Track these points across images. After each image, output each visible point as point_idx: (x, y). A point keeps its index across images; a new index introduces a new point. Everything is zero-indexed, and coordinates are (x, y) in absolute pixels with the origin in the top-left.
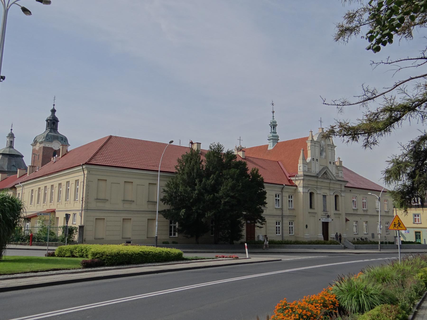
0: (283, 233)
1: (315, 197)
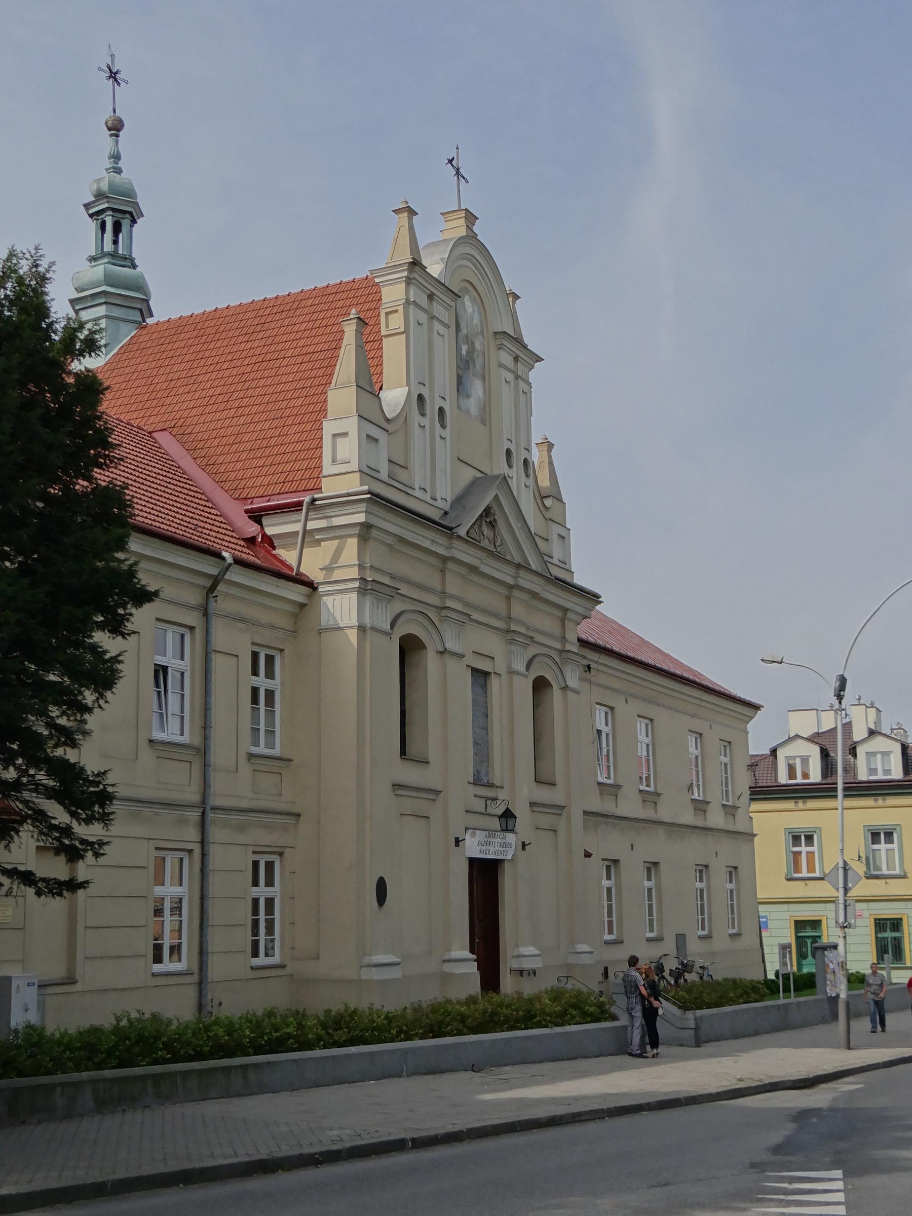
0: (202, 952)
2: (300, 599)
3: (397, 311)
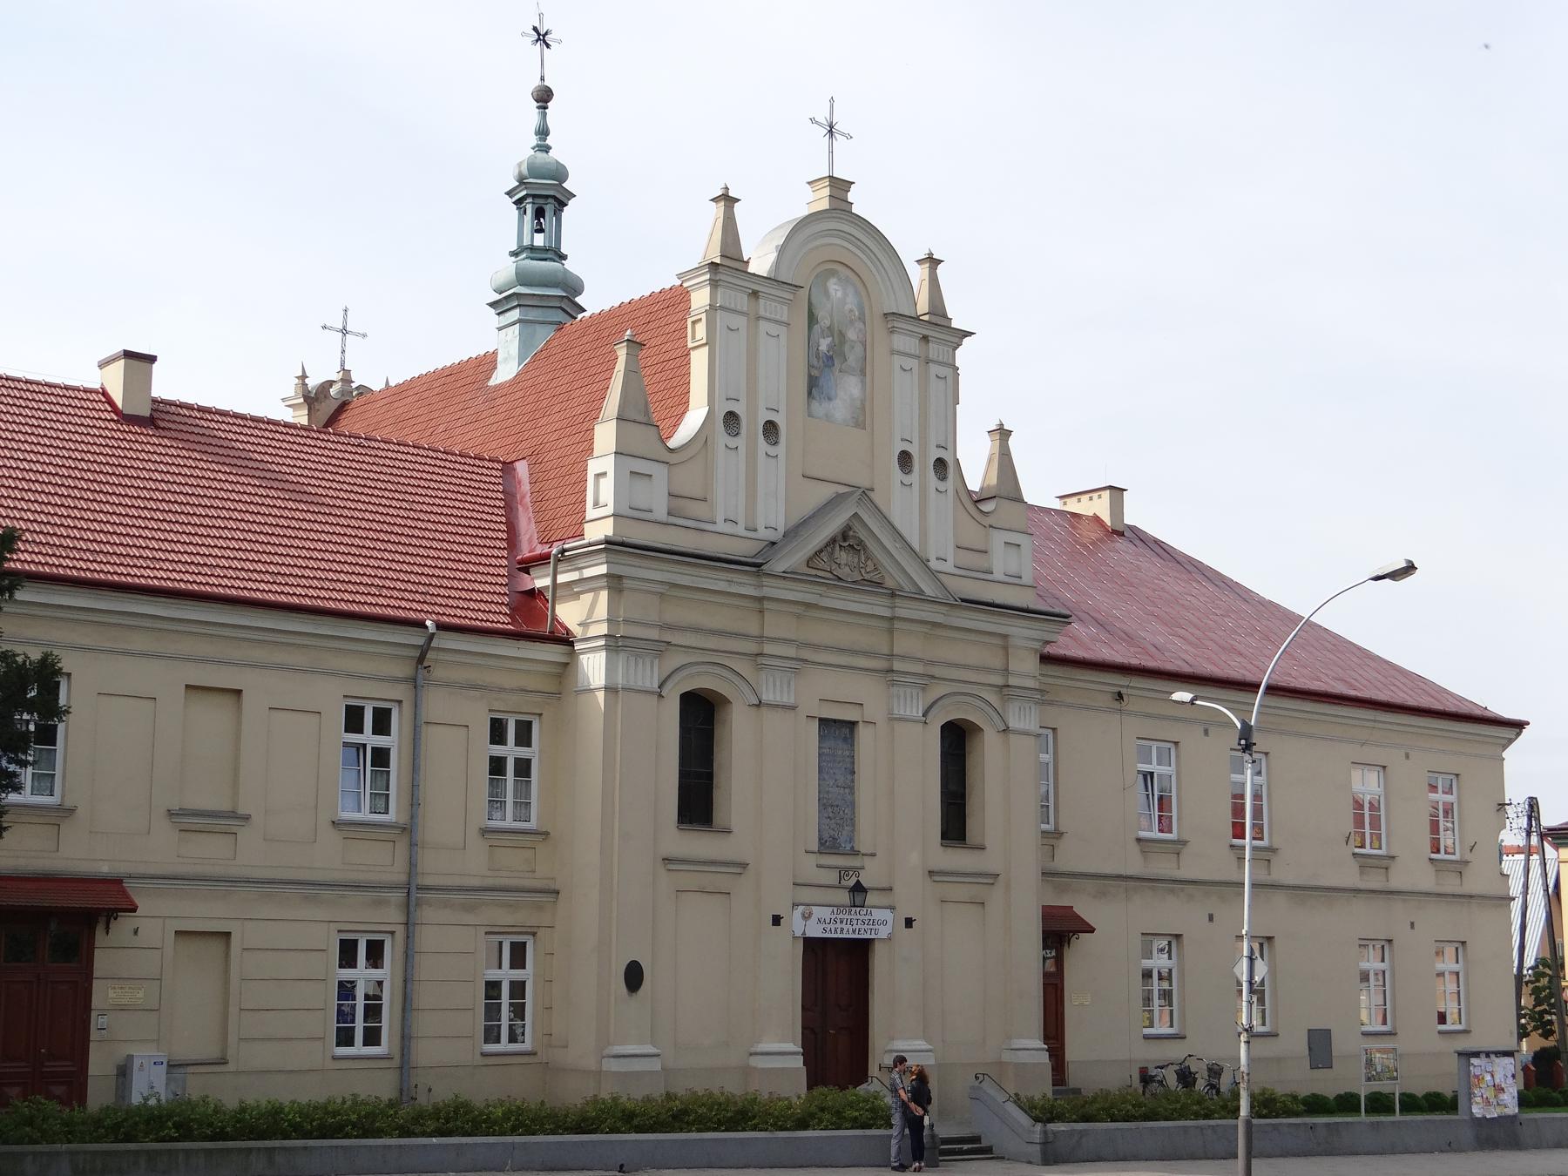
1: (740, 736)
2: (563, 659)
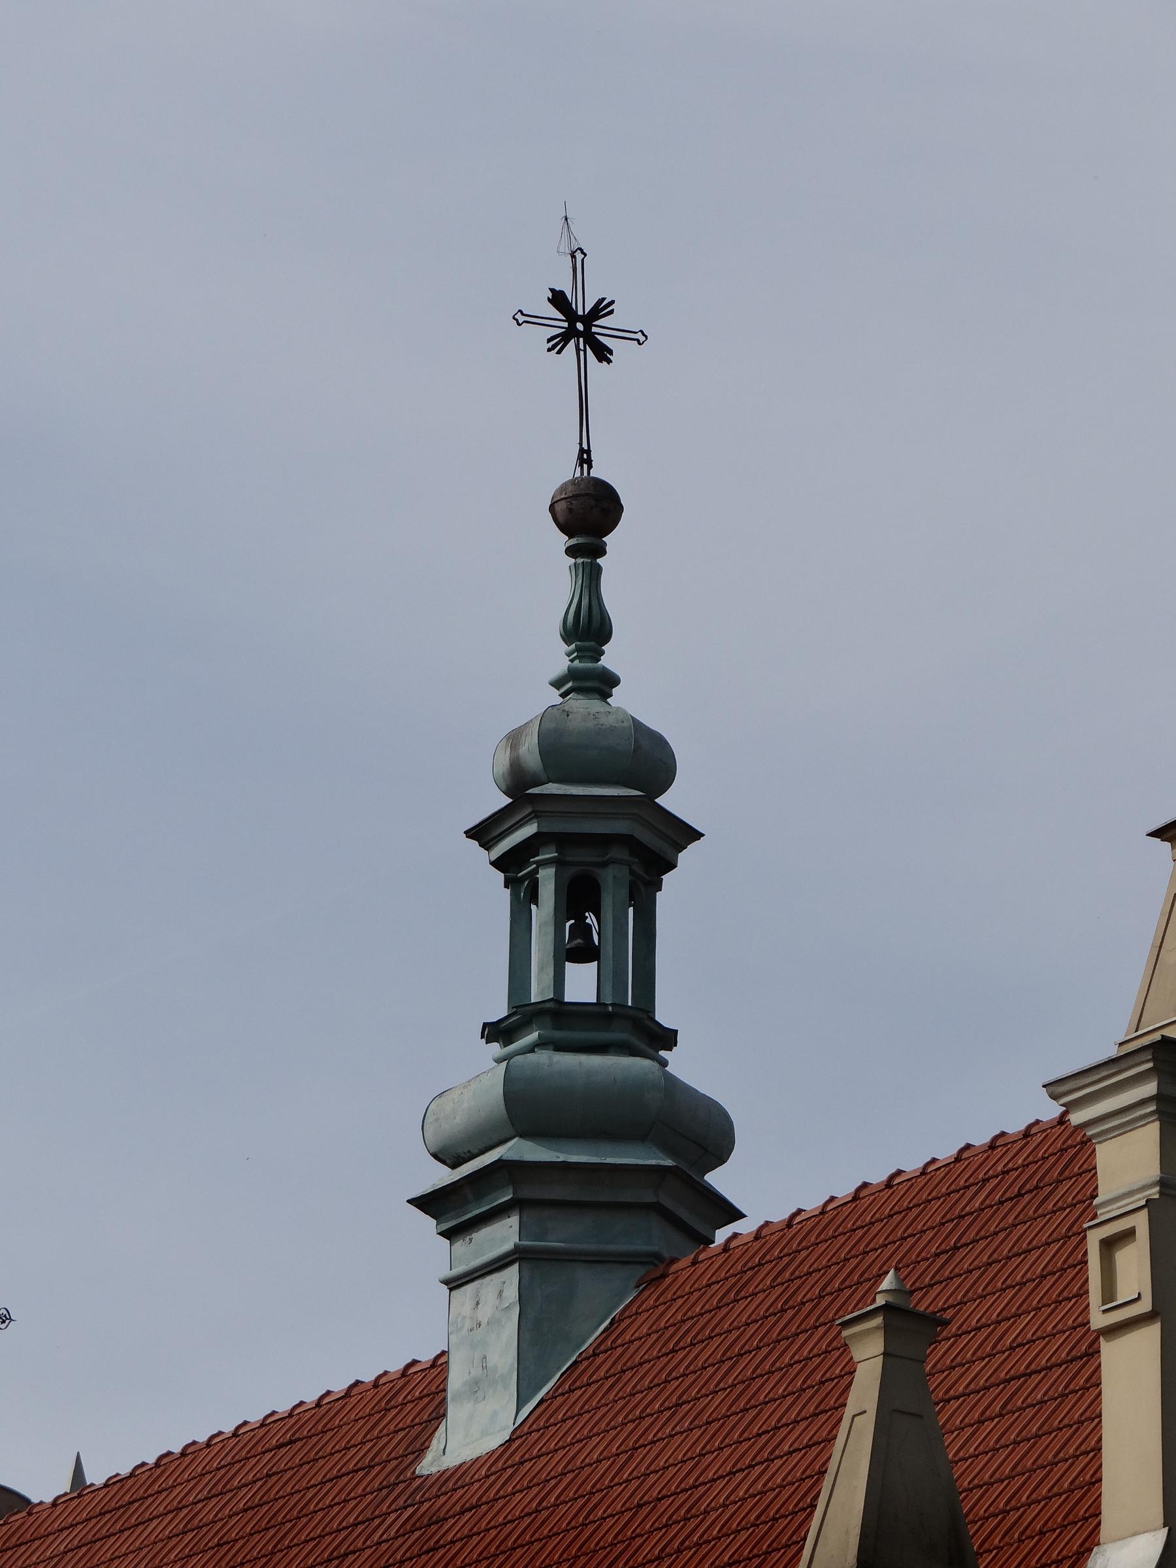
3: (1130, 1234)
